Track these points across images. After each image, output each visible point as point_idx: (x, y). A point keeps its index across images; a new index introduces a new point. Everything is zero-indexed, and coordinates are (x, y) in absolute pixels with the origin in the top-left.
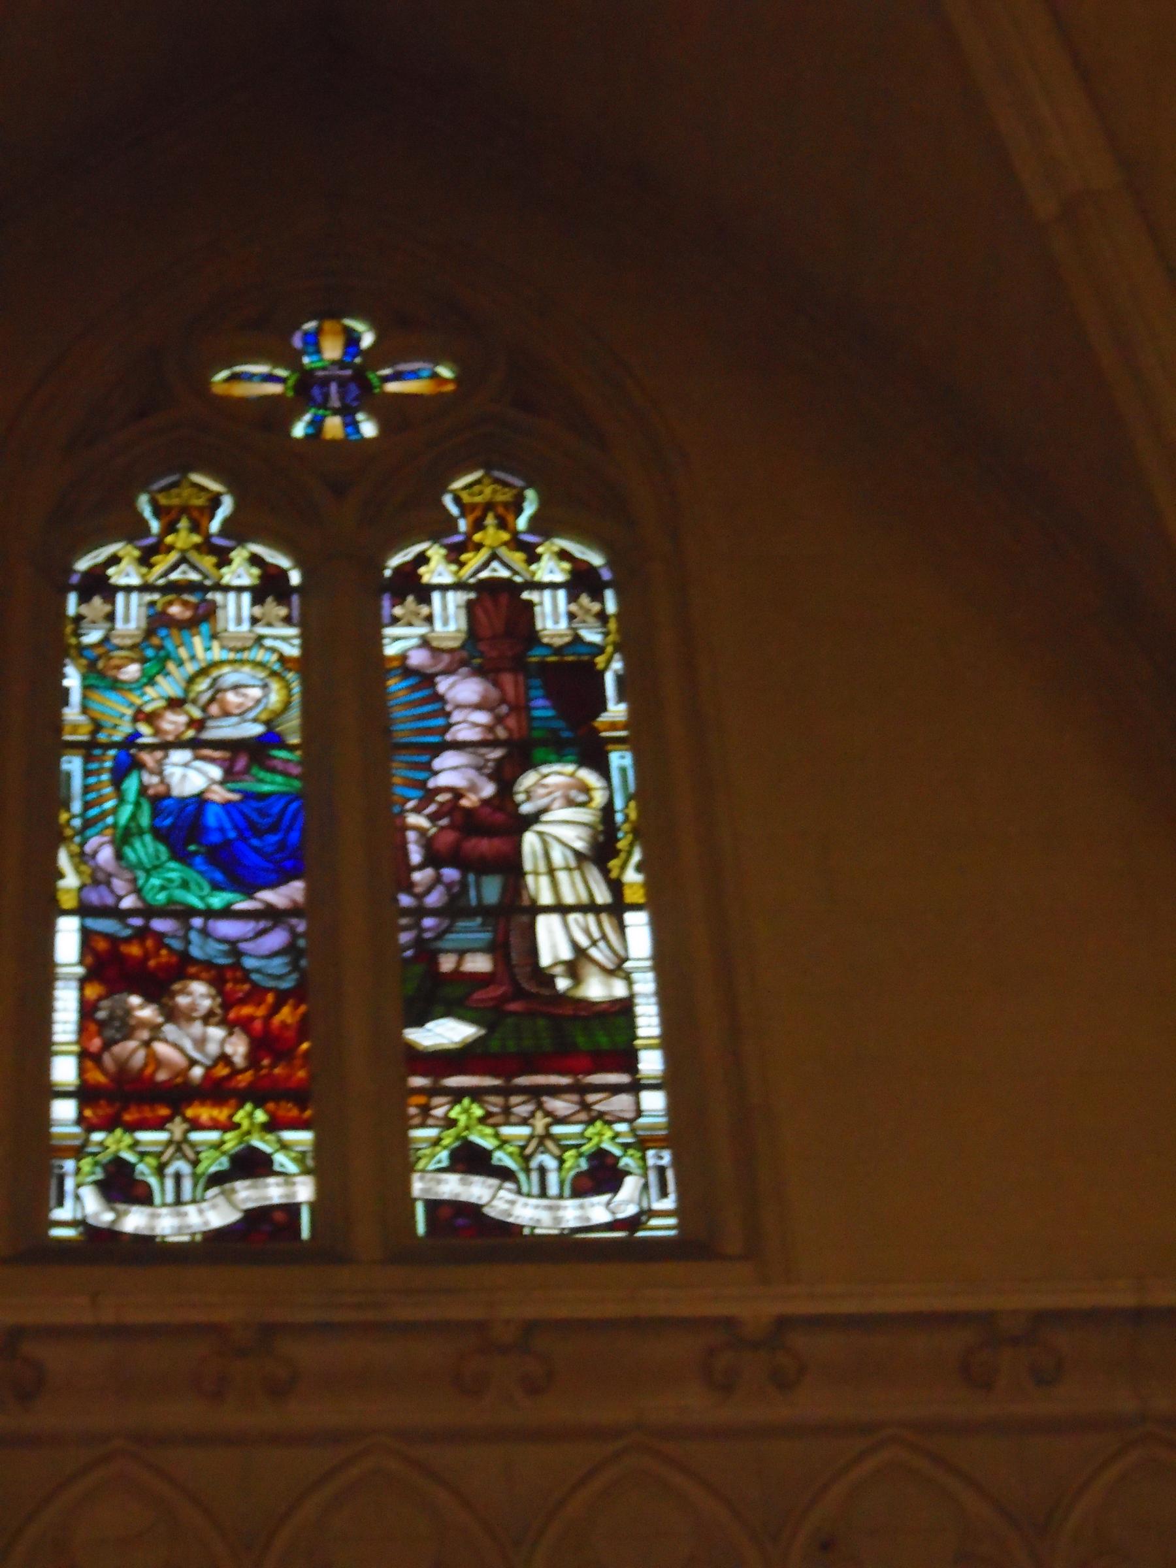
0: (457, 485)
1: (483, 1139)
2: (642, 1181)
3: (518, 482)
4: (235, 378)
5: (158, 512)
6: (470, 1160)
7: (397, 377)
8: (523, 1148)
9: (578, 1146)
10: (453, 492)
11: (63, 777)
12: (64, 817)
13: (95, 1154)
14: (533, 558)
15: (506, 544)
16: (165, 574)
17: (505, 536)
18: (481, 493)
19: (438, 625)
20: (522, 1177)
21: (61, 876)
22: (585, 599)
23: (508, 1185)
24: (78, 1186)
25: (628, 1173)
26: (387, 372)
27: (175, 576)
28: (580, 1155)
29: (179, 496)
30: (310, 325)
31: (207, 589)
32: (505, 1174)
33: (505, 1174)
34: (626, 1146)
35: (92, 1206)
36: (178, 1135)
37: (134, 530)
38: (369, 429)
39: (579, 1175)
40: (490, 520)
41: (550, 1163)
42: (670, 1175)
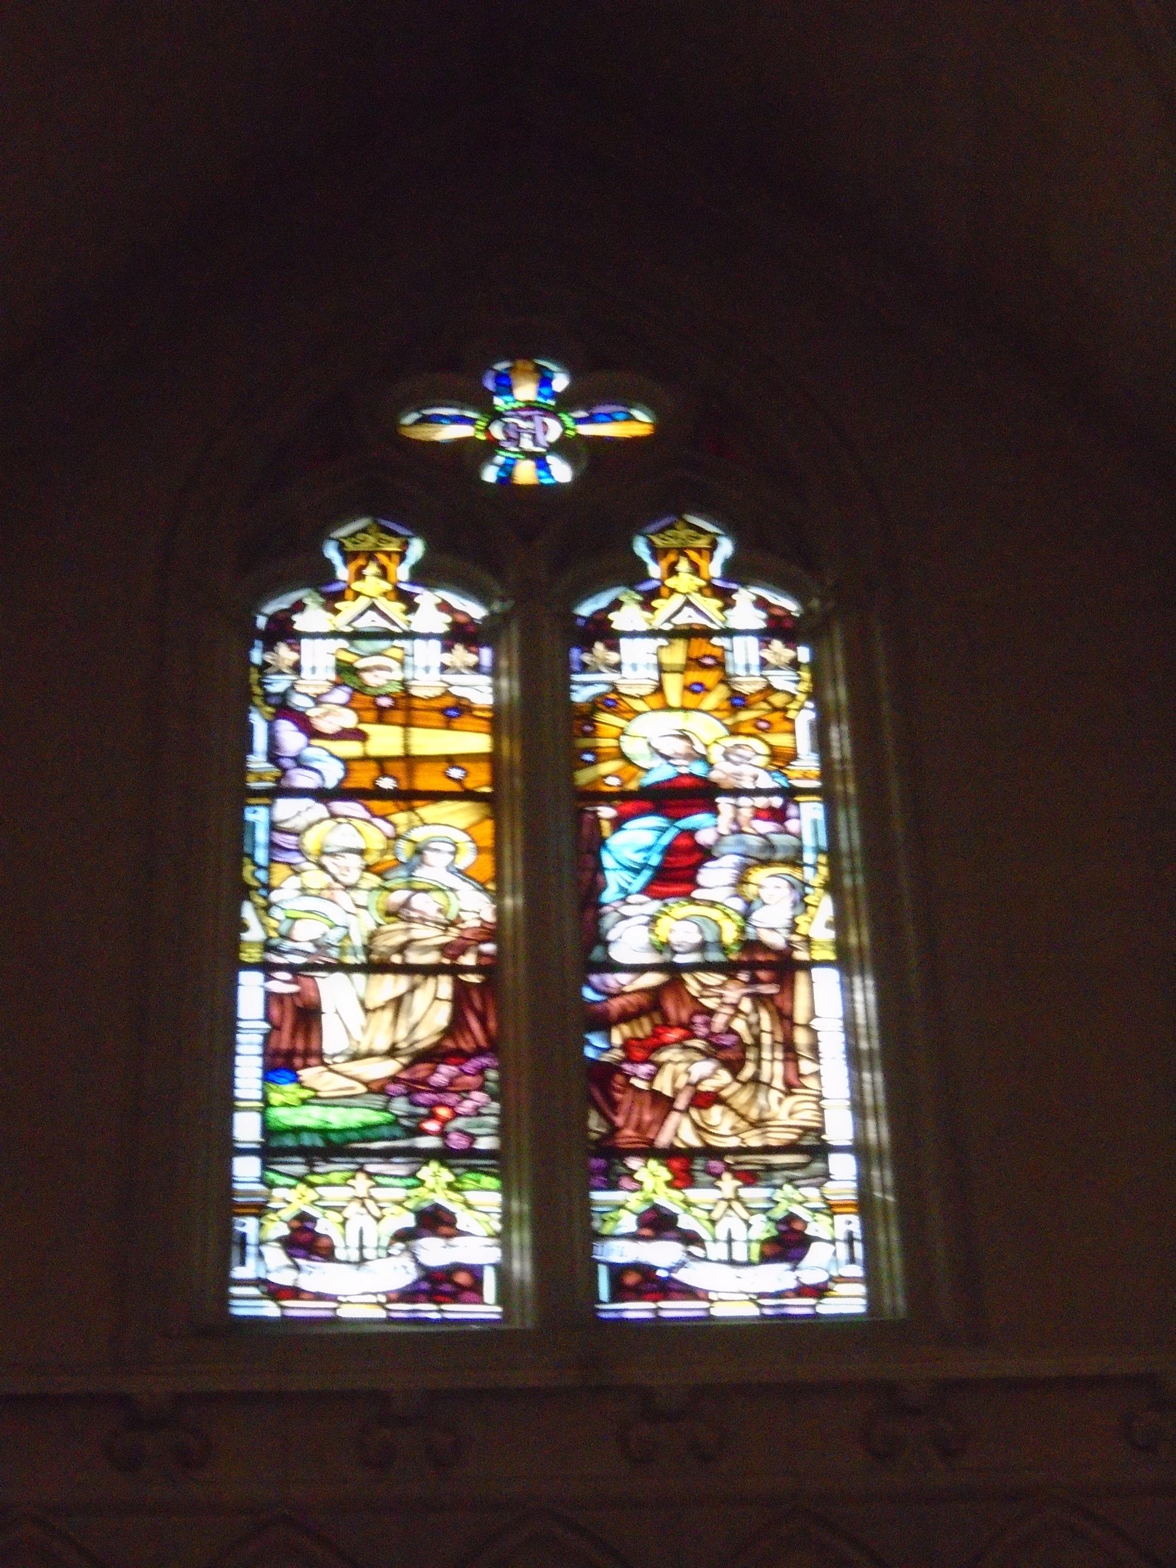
1: (670, 1200)
4: (425, 420)
5: (348, 557)
6: (658, 1223)
12: (247, 870)
14: (728, 605)
15: (385, 594)
17: (387, 586)
21: (245, 928)
29: (675, 537)
30: (501, 366)
33: (690, 1238)
34: (815, 1210)
35: (276, 1265)
37: (634, 574)
39: (764, 1243)
40: (683, 566)
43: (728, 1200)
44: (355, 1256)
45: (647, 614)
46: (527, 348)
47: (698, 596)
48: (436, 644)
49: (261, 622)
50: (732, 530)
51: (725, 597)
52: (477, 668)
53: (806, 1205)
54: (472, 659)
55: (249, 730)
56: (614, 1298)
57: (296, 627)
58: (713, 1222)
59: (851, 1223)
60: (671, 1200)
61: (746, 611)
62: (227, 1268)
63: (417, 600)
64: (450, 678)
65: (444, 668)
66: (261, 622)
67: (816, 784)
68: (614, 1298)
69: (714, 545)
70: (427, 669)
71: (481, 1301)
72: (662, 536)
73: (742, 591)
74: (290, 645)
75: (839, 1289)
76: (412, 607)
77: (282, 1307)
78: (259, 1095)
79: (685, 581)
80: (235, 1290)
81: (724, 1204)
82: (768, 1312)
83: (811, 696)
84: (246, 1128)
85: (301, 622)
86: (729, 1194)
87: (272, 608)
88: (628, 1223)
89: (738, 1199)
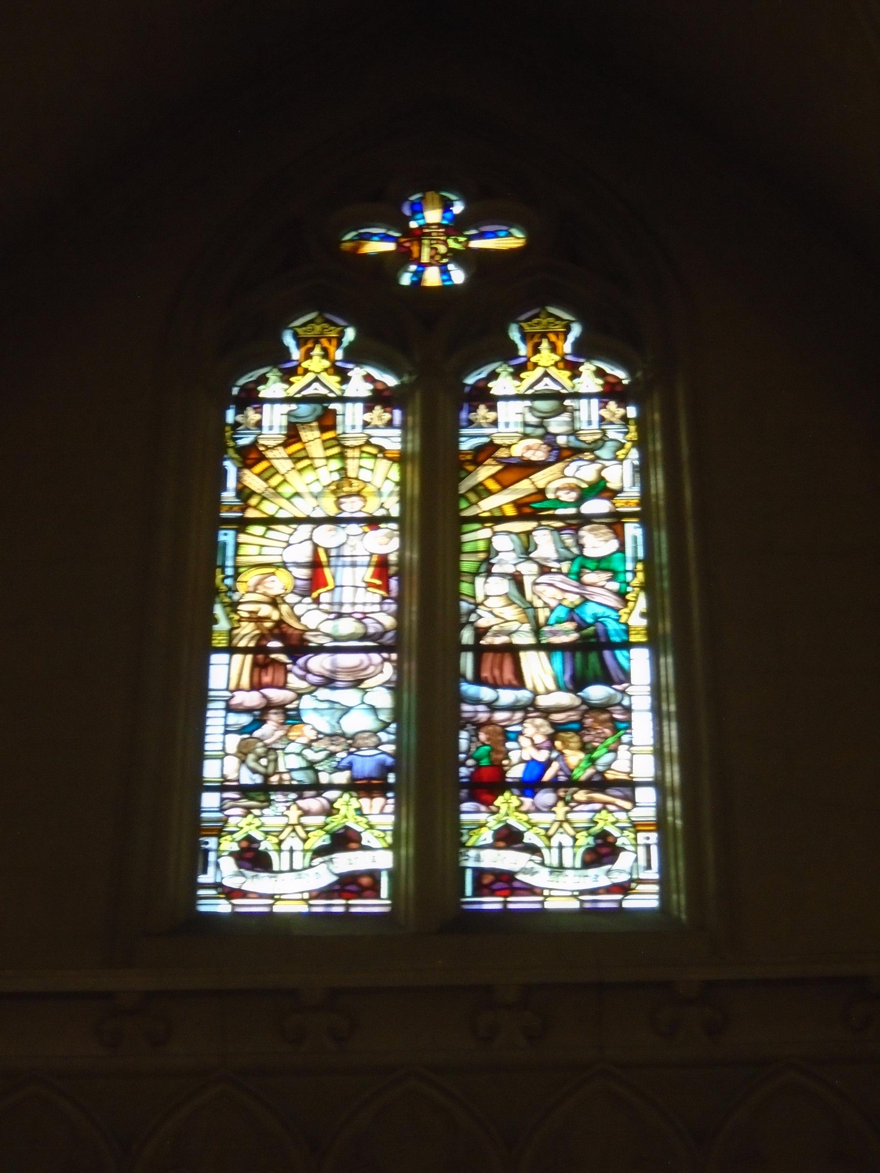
1: (516, 821)
5: (525, 337)
7: (482, 236)
8: (547, 830)
9: (588, 829)
10: (292, 328)
11: (220, 545)
13: (232, 833)
14: (576, 375)
15: (326, 370)
16: (531, 387)
17: (326, 364)
18: (538, 324)
20: (545, 851)
22: (612, 405)
23: (535, 858)
24: (219, 857)
25: (623, 849)
26: (473, 232)
27: (540, 387)
30: (414, 198)
32: (533, 850)
33: (533, 850)
34: (622, 829)
37: (508, 352)
38: (458, 276)
41: (567, 841)
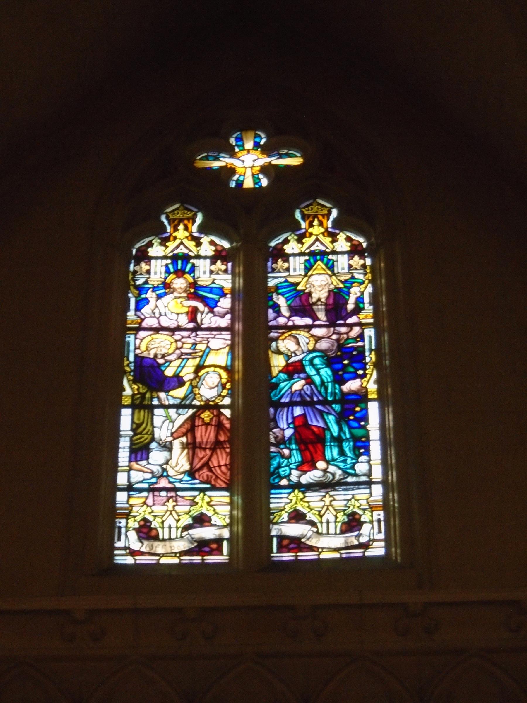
0: (169, 210)
2: (371, 525)
3: (328, 205)
6: (297, 517)
8: (320, 512)
10: (166, 213)
13: (135, 517)
14: (334, 240)
15: (187, 237)
17: (322, 230)
19: (292, 272)
20: (319, 525)
28: (135, 521)
31: (328, 254)
33: (313, 524)
34: (364, 510)
36: (171, 508)
37: (296, 227)
39: (344, 523)
40: (316, 222)
42: (382, 523)
43: (171, 511)
44: (334, 533)
45: (300, 245)
46: (248, 125)
47: (186, 240)
48: (208, 261)
49: (134, 251)
50: (336, 205)
51: (334, 237)
52: (226, 271)
53: (361, 507)
54: (224, 267)
55: (128, 300)
56: (278, 552)
57: (149, 254)
58: (321, 517)
59: (379, 515)
60: (303, 507)
61: (342, 244)
62: (113, 542)
63: (201, 241)
64: (214, 276)
65: (211, 272)
66: (134, 251)
67: (371, 321)
68: (278, 552)
69: (330, 213)
70: (205, 273)
71: (222, 554)
72: (307, 209)
73: (341, 233)
74: (146, 262)
75: (375, 544)
76: (199, 244)
77: (135, 560)
78: (127, 464)
79: (181, 233)
80: (116, 552)
81: (168, 513)
82: (344, 556)
83: (370, 281)
84: (122, 479)
85: (152, 252)
86: (328, 503)
87: (138, 246)
88: (285, 516)
89: (331, 505)
